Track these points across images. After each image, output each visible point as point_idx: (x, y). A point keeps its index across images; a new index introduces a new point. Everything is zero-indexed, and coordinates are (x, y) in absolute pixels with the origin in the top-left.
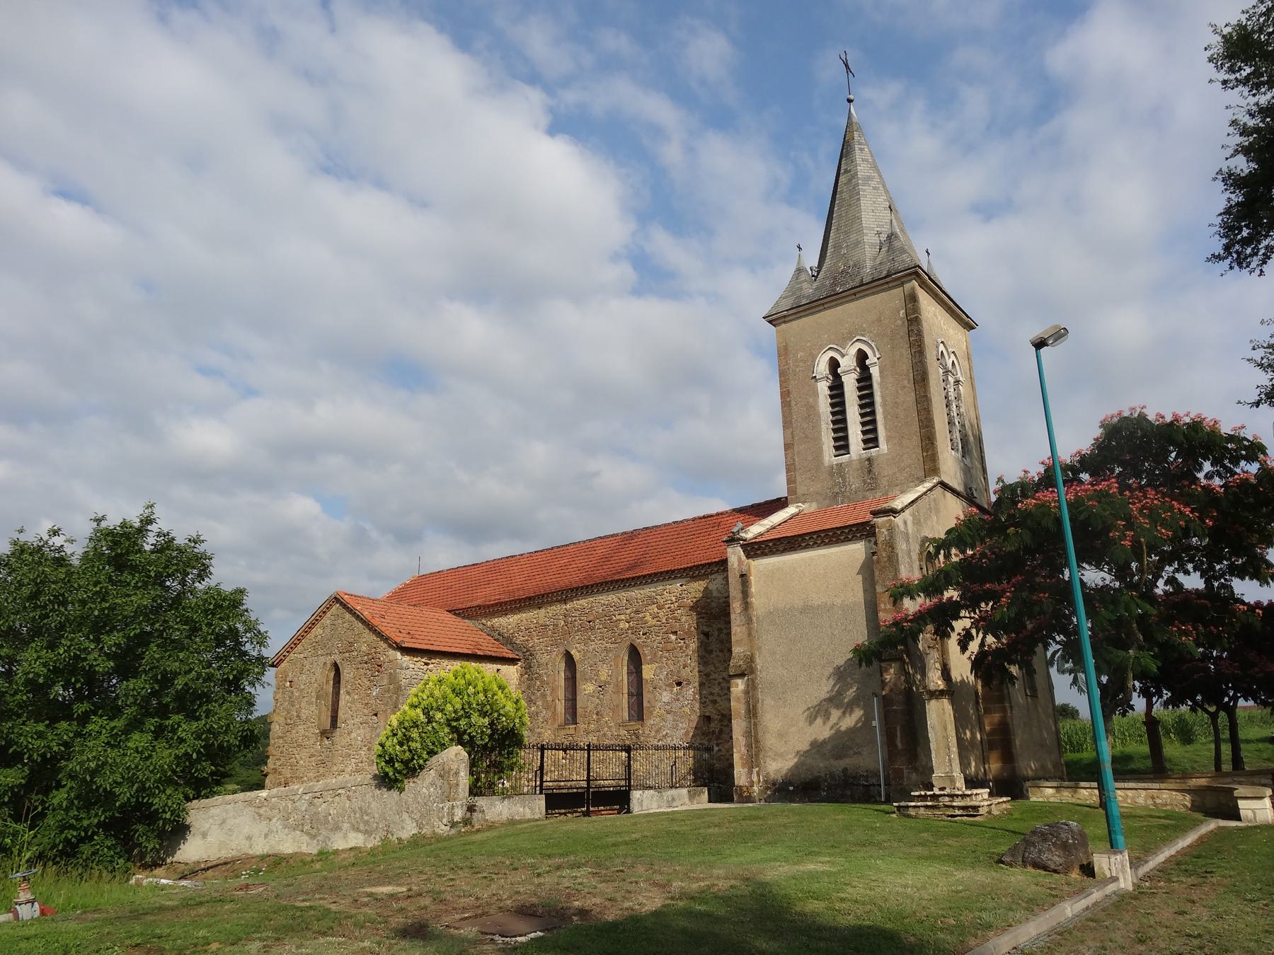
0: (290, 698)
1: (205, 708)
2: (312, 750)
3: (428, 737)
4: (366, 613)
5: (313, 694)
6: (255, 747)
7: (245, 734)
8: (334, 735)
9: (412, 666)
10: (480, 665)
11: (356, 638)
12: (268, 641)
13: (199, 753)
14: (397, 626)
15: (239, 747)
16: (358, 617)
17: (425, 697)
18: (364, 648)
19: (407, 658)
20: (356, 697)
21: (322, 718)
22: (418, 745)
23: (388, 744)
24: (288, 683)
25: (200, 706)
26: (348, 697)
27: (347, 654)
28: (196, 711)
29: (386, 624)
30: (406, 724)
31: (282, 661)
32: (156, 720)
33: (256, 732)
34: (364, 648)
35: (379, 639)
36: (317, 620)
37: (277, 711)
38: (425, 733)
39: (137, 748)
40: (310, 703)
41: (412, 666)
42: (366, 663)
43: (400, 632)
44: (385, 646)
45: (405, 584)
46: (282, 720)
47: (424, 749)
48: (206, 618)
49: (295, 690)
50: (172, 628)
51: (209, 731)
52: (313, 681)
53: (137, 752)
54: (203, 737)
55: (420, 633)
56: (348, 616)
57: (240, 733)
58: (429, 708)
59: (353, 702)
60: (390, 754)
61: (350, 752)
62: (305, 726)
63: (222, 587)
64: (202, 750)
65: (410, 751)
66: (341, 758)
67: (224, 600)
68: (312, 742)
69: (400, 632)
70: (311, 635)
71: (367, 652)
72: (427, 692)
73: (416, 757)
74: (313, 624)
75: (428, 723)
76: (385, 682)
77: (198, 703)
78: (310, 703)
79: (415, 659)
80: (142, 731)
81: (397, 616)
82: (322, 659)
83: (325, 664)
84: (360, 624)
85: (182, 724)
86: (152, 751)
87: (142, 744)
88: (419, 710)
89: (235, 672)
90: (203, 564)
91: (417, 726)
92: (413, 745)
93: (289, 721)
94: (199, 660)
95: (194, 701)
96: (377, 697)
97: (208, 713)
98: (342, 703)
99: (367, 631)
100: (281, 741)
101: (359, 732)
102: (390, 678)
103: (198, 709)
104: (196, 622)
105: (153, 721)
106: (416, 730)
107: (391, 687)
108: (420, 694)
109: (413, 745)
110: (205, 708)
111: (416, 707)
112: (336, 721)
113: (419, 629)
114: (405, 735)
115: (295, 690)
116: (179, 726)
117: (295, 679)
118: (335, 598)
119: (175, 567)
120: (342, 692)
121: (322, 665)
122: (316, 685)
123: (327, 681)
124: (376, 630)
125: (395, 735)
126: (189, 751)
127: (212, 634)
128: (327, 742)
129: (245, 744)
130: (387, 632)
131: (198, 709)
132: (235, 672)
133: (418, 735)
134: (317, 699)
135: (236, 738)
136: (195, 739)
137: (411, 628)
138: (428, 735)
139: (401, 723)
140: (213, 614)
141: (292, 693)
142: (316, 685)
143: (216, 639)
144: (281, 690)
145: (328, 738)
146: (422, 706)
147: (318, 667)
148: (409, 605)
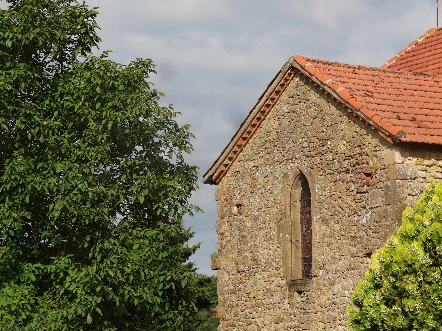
0: (240, 230)
1: (99, 246)
2: (279, 312)
3: (435, 290)
4: (340, 89)
5: (272, 224)
6: (187, 307)
7: (167, 287)
8: (307, 288)
9: (423, 174)
10: (326, 104)
11: (330, 132)
12: (192, 141)
13: (95, 315)
14: (395, 109)
15: (162, 306)
16: (329, 97)
17: (426, 221)
18: (343, 147)
19: (411, 161)
20: (337, 227)
21: (289, 261)
22: (417, 304)
23: (367, 302)
24: (235, 209)
25: (92, 243)
26: (324, 227)
27: (318, 159)
28: (87, 251)
29: (375, 106)
30: (396, 268)
31: (223, 174)
32: (37, 265)
33: (183, 284)
34: (343, 147)
35: (364, 132)
36: (268, 106)
37: (224, 250)
38: (430, 283)
39: (9, 306)
40: (269, 238)
41: (423, 174)
42: (347, 172)
43: (399, 118)
44: (375, 141)
45: (417, 44)
46: (231, 266)
47: (428, 311)
48: (93, 108)
49: (246, 219)
50: (39, 125)
51: (105, 281)
52: (271, 203)
53: (11, 313)
54: (98, 289)
55: (433, 118)
56: (314, 96)
57: (161, 286)
58: (435, 240)
59: (332, 235)
60: (372, 320)
61: (335, 315)
62: (265, 274)
63: (111, 57)
64: (99, 310)
65: (405, 314)
66: (322, 325)
67: (115, 78)
68: (277, 298)
69: (399, 118)
70: (261, 132)
71: (348, 153)
72: (430, 213)
73: (415, 325)
74: (263, 112)
75: (434, 265)
76: (380, 201)
77: (88, 239)
78: (269, 238)
79: (427, 162)
80: (19, 282)
81: (395, 92)
82: (281, 169)
83: (286, 175)
84: (334, 109)
85: (70, 271)
86: (32, 312)
87: (16, 301)
88: (415, 244)
89: (146, 192)
90: (84, 25)
91: (415, 272)
92: (409, 303)
93: (241, 266)
94: (83, 173)
95: (84, 236)
96: (368, 227)
97: (105, 253)
98: (316, 237)
99: (345, 119)
100: (233, 298)
101: (344, 281)
102: (386, 194)
103: (89, 247)
104: (80, 116)
105: (33, 267)
106: (412, 278)
107: (390, 209)
108: (418, 216)
109: (409, 303)
110: (99, 246)
111: (412, 238)
112: (310, 266)
113: (431, 112)
114: (395, 288)
115: (246, 219)
116: (66, 274)
117: (245, 202)
118: (292, 68)
119: (38, 30)
120: (315, 219)
121: (281, 178)
122: (275, 210)
123: (292, 203)
124: (358, 116)
125: (378, 287)
126: (80, 311)
127: (103, 132)
128: (299, 300)
129: (171, 305)
130: (376, 119)
131: (89, 247)
132: (146, 192)
133: (416, 286)
134: (279, 231)
135: (156, 294)
136: (86, 293)
137: (418, 111)
138: (434, 286)
139: (387, 267)
140: (104, 102)
141: (242, 223)
142: (275, 210)
143: (112, 138)
144: (226, 220)
145: (300, 293)
146: (422, 237)
147: (276, 182)
148: (415, 74)
